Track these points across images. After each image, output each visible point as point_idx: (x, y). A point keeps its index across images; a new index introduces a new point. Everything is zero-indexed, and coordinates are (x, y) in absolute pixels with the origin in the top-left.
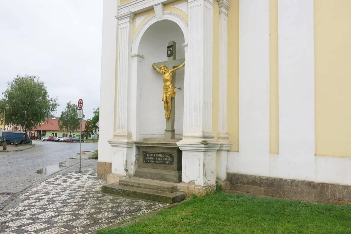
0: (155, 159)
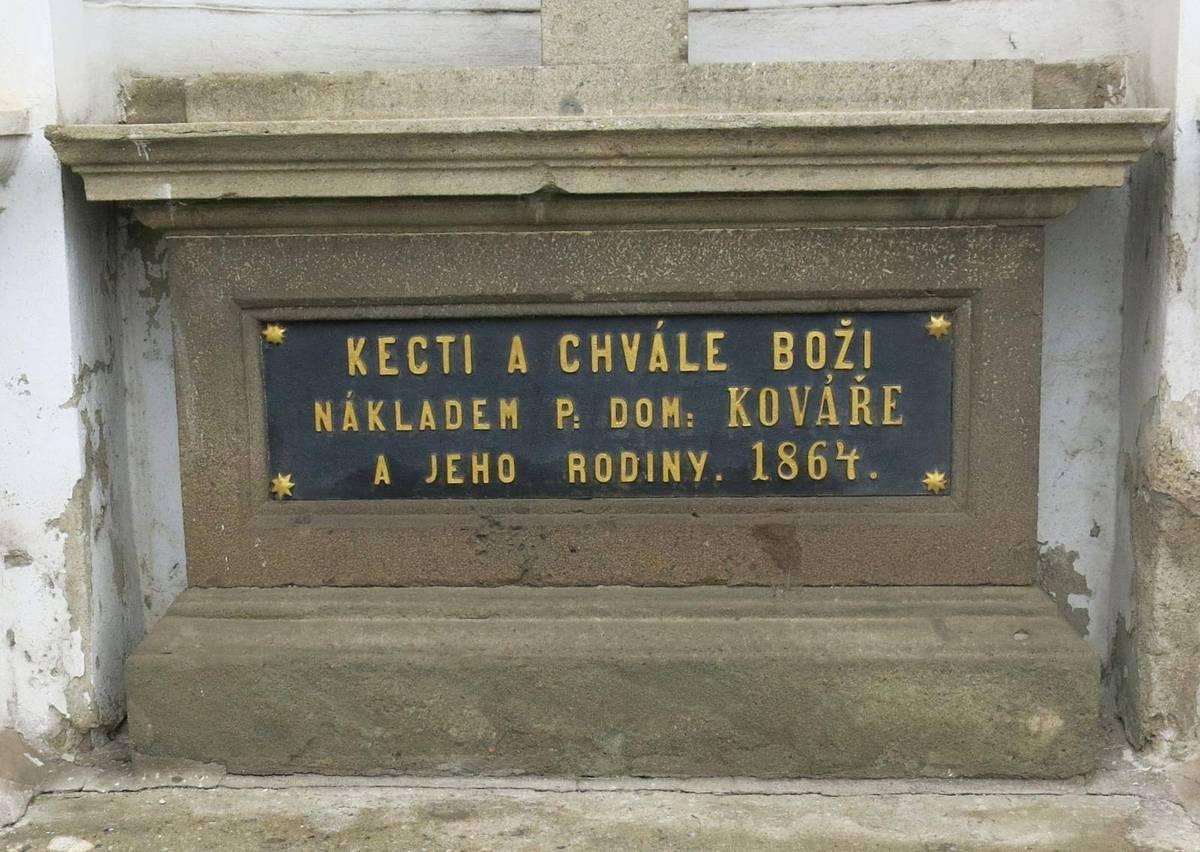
0: (537, 412)
